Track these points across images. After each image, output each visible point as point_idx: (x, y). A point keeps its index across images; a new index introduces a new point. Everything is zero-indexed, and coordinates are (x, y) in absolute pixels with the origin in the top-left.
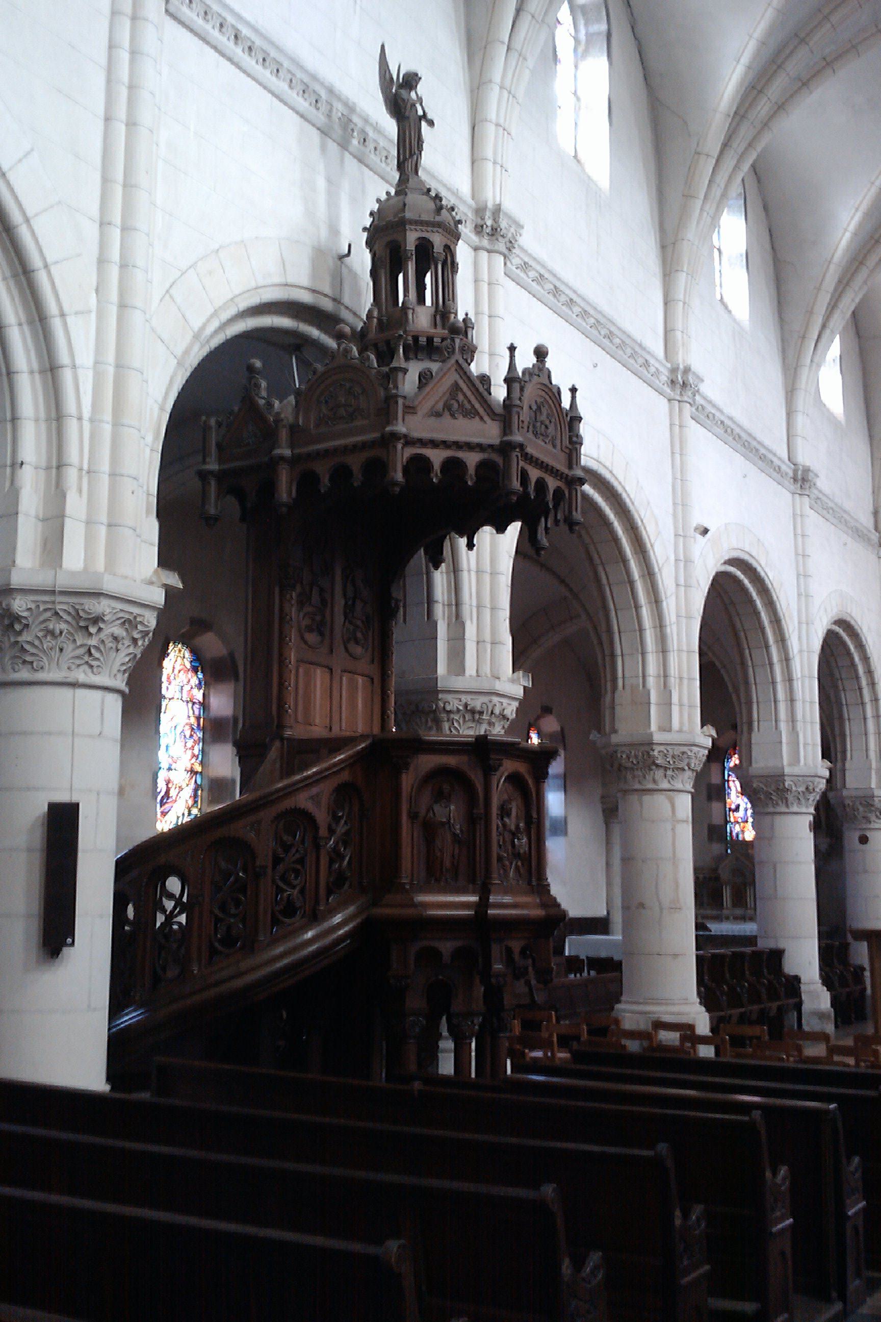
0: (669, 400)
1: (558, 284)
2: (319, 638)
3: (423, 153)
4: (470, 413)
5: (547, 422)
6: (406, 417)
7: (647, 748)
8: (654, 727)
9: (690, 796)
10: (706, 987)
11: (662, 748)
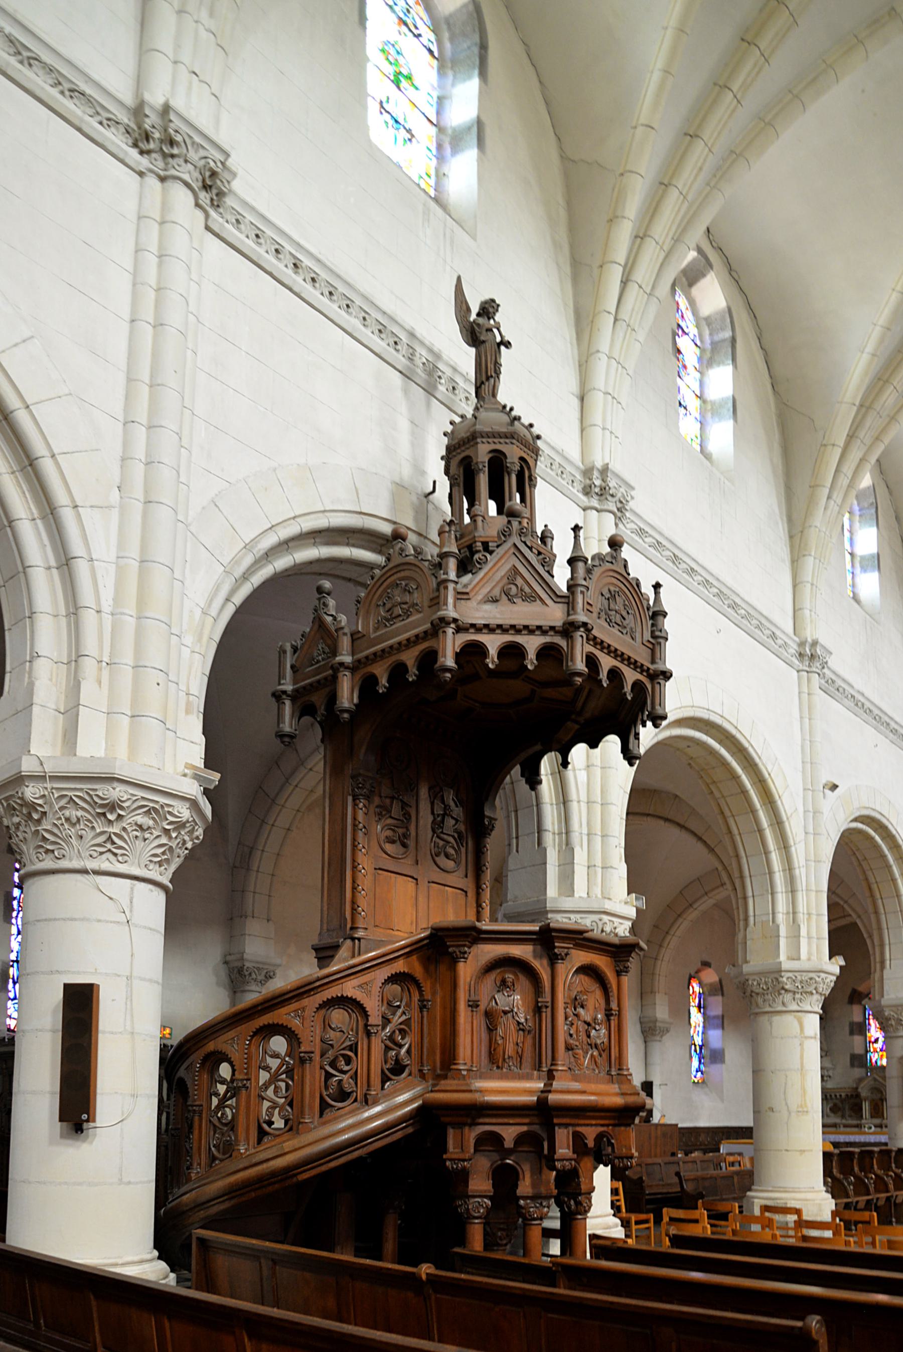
0: (798, 671)
1: (677, 552)
2: (402, 850)
3: (501, 377)
4: (532, 597)
5: (624, 614)
6: (457, 605)
7: (776, 975)
8: (783, 957)
9: (818, 1017)
10: (834, 1179)
11: (790, 975)
